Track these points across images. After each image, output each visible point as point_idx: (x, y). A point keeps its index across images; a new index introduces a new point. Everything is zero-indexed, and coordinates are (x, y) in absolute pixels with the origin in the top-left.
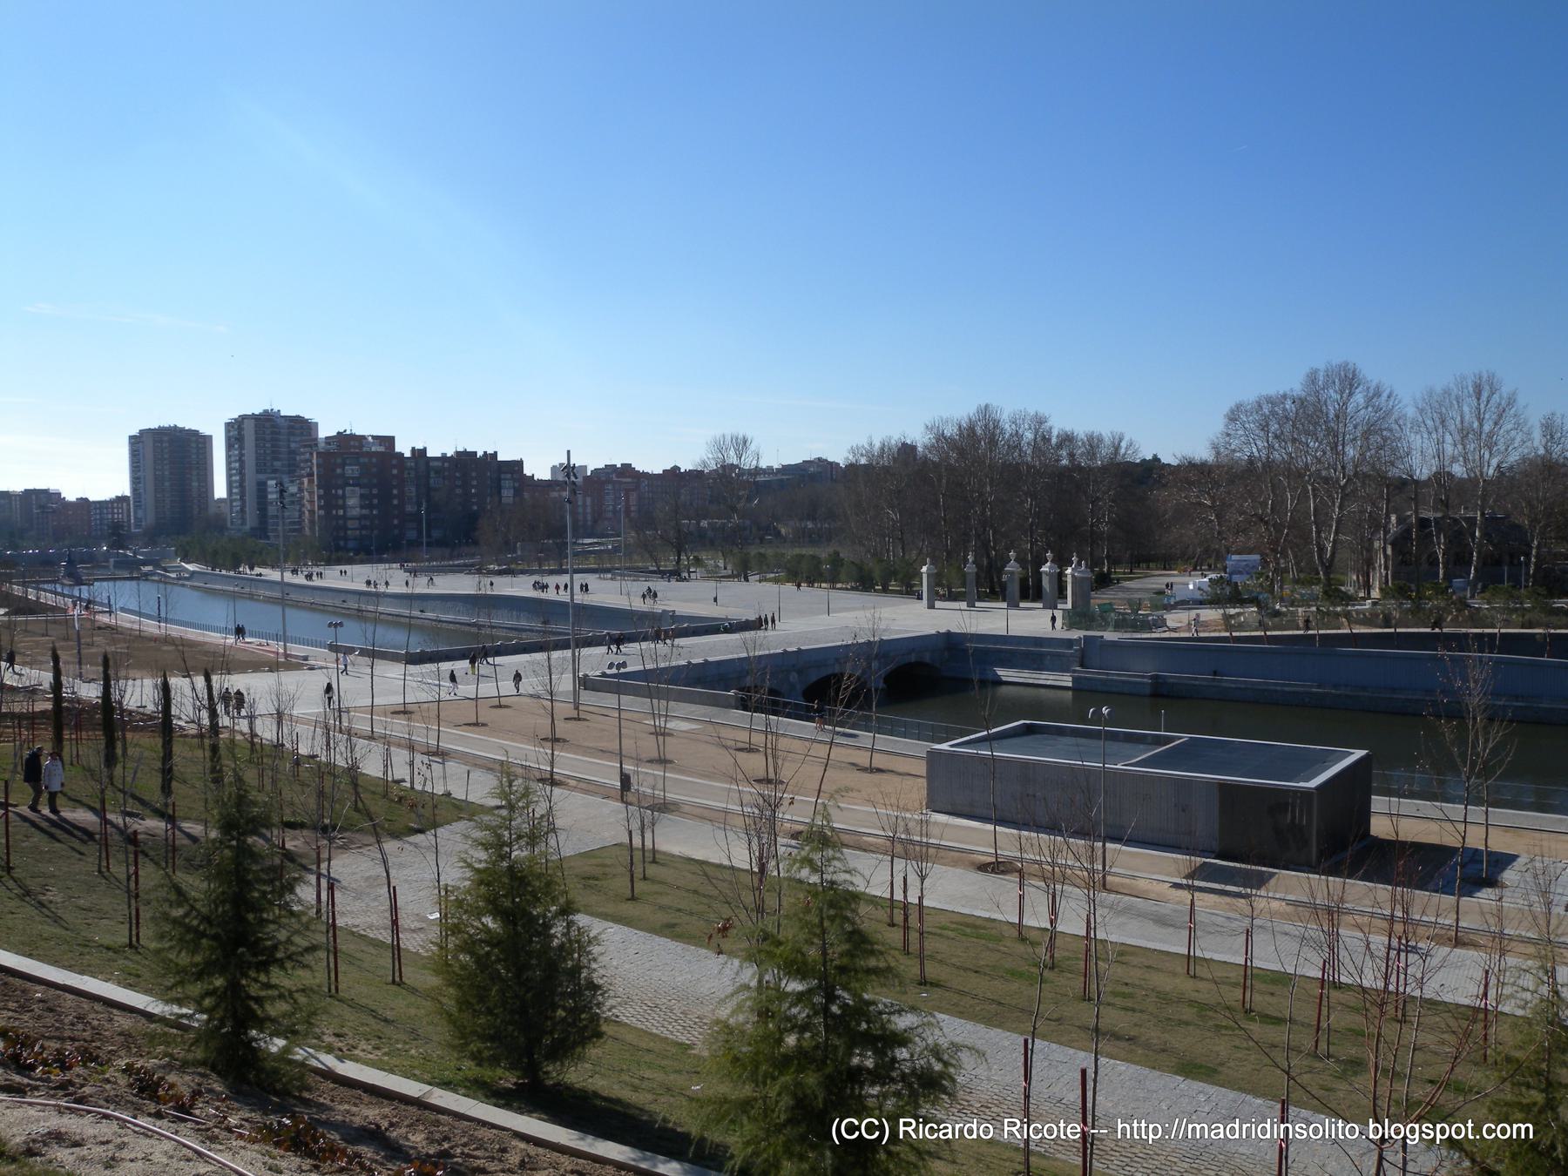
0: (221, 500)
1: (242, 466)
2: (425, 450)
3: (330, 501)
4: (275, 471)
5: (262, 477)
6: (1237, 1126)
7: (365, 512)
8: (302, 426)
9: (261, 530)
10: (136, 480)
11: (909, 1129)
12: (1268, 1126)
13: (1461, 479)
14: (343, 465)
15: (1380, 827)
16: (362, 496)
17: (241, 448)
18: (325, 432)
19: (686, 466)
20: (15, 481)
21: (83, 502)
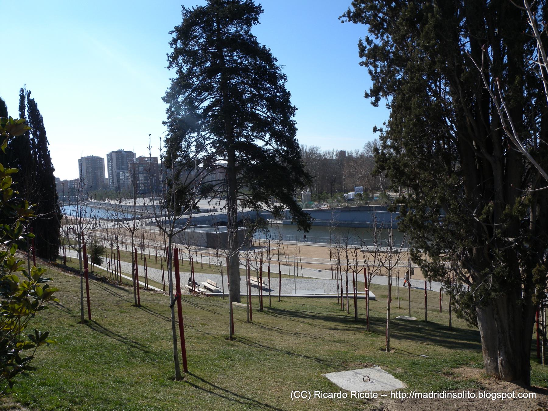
0: (107, 179)
1: (112, 168)
3: (134, 177)
4: (123, 169)
5: (118, 171)
6: (432, 394)
8: (131, 154)
9: (118, 189)
10: (81, 174)
11: (318, 395)
12: (443, 394)
13: (395, 125)
14: (139, 167)
17: (112, 162)
18: (138, 156)
19: (52, 161)
21: (66, 181)
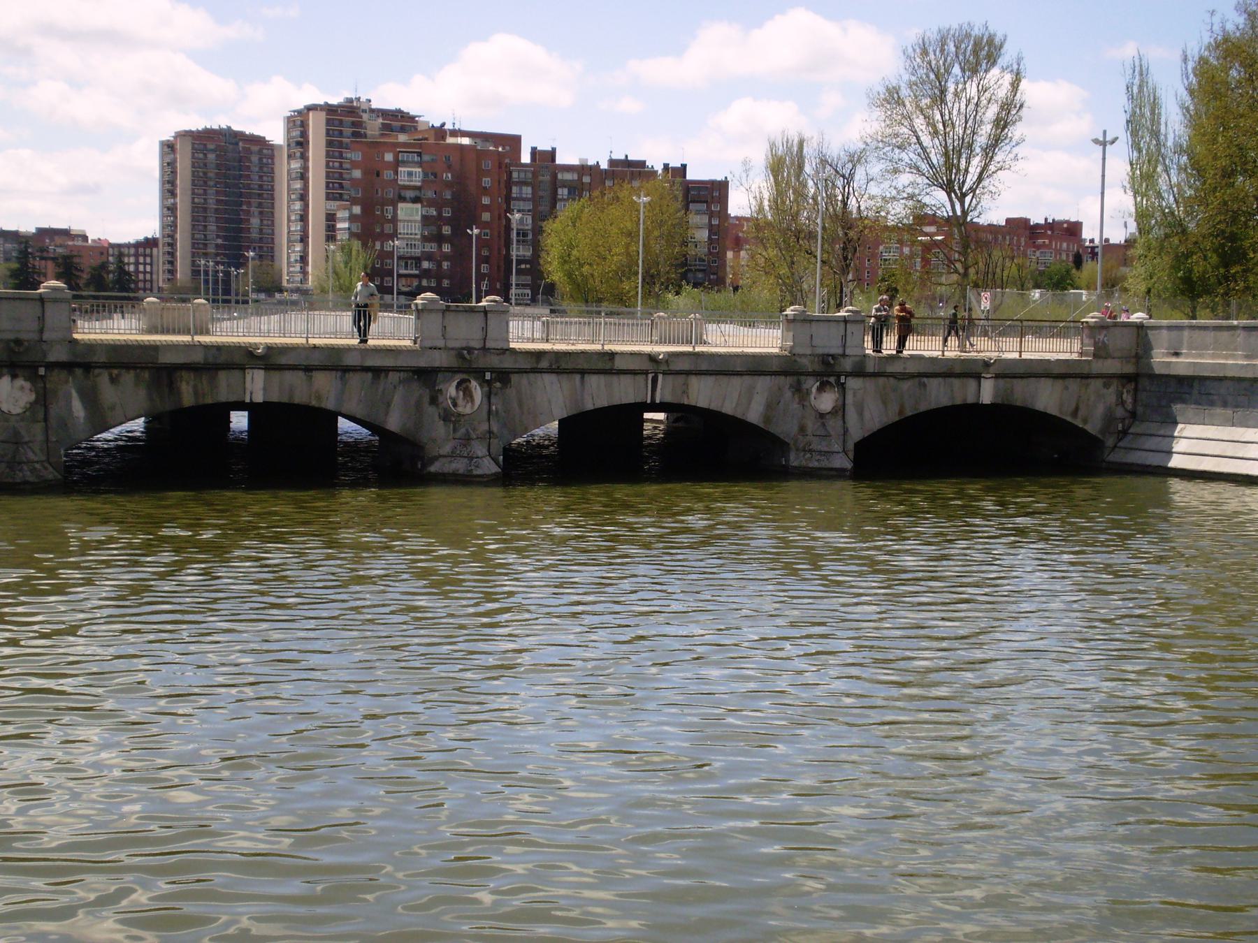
2: (552, 154)
5: (333, 205)
7: (431, 247)
10: (169, 210)
14: (397, 163)
15: (529, 278)
16: (426, 220)
17: (304, 157)
20: (25, 217)
